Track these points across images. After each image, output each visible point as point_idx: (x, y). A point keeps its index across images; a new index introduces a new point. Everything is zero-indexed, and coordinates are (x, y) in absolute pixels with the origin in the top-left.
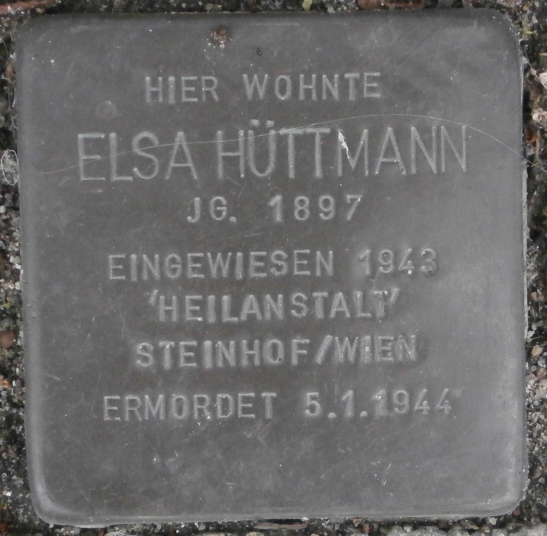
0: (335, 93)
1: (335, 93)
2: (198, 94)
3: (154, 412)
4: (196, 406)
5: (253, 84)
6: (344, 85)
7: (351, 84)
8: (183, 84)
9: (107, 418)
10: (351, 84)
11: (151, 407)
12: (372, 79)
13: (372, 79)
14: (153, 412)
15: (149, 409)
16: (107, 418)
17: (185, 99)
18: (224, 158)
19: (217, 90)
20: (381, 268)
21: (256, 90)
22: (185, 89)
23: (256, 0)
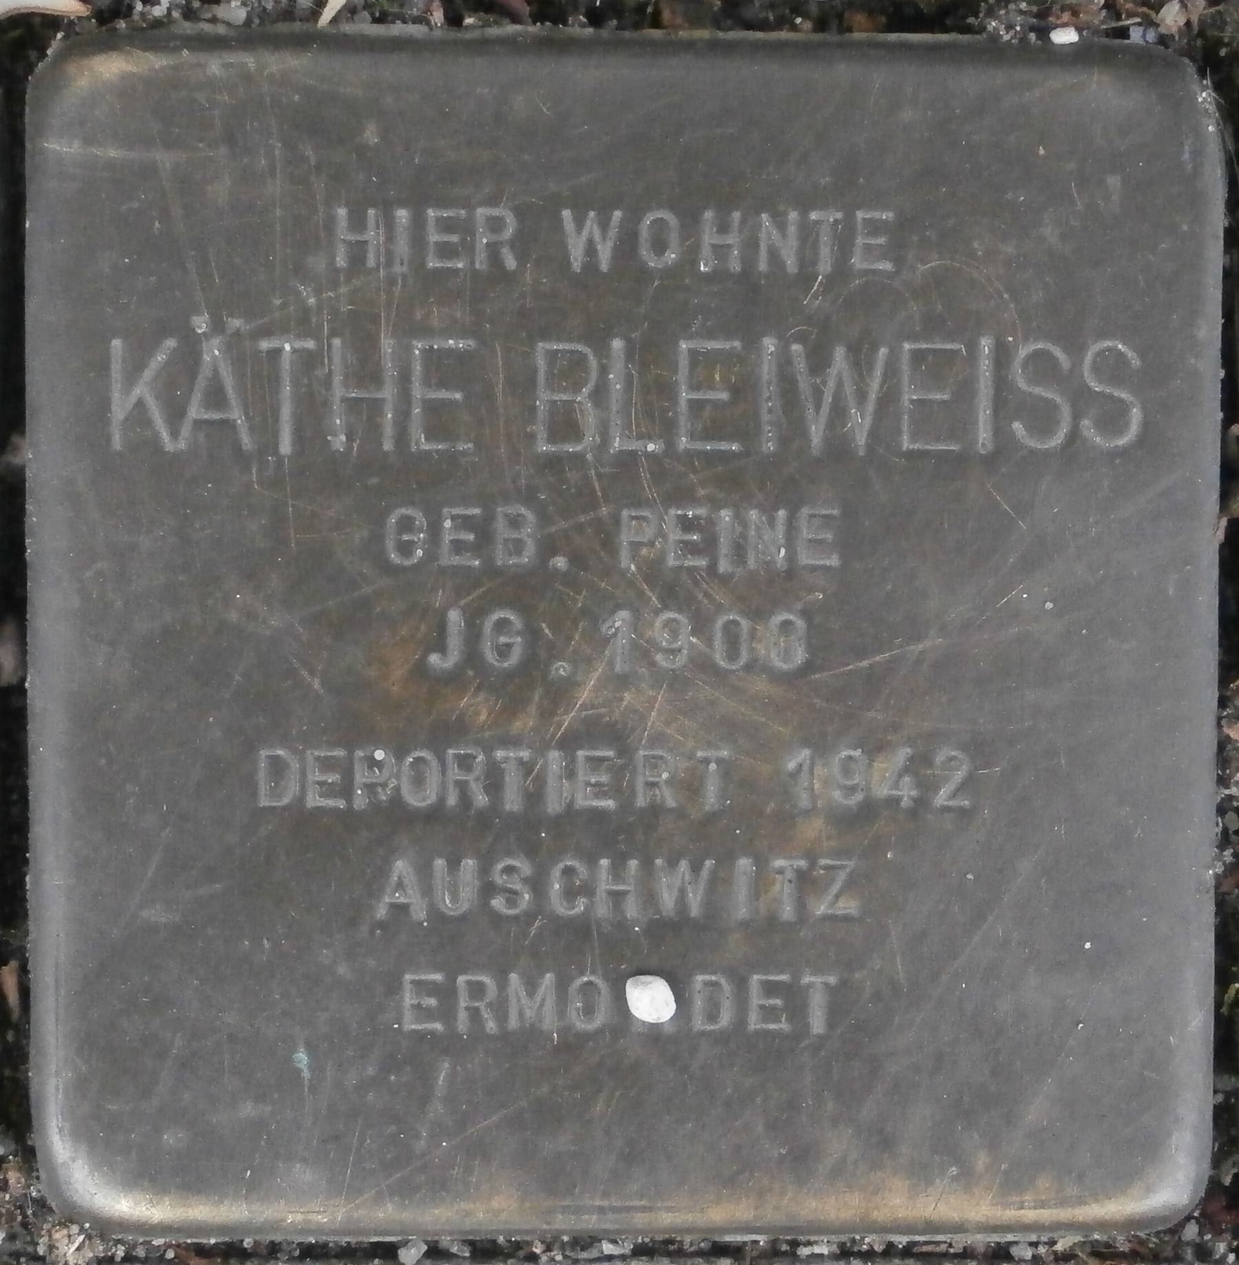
5: (585, 233)
12: (874, 227)
13: (874, 227)
21: (591, 250)
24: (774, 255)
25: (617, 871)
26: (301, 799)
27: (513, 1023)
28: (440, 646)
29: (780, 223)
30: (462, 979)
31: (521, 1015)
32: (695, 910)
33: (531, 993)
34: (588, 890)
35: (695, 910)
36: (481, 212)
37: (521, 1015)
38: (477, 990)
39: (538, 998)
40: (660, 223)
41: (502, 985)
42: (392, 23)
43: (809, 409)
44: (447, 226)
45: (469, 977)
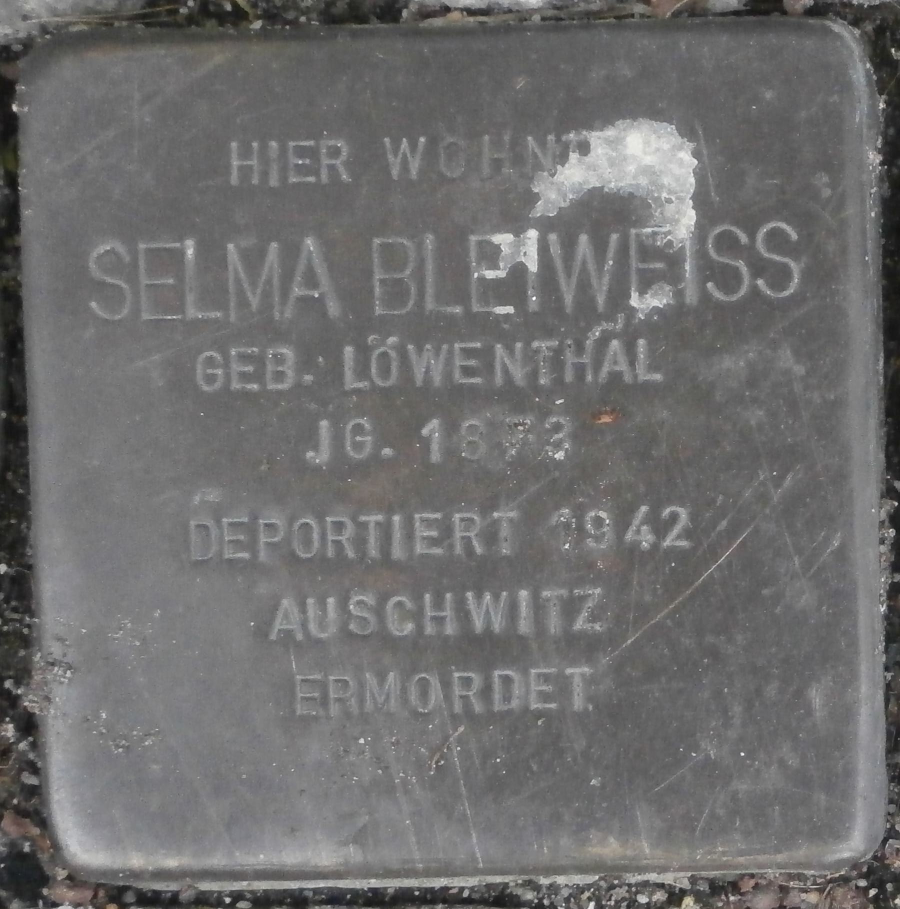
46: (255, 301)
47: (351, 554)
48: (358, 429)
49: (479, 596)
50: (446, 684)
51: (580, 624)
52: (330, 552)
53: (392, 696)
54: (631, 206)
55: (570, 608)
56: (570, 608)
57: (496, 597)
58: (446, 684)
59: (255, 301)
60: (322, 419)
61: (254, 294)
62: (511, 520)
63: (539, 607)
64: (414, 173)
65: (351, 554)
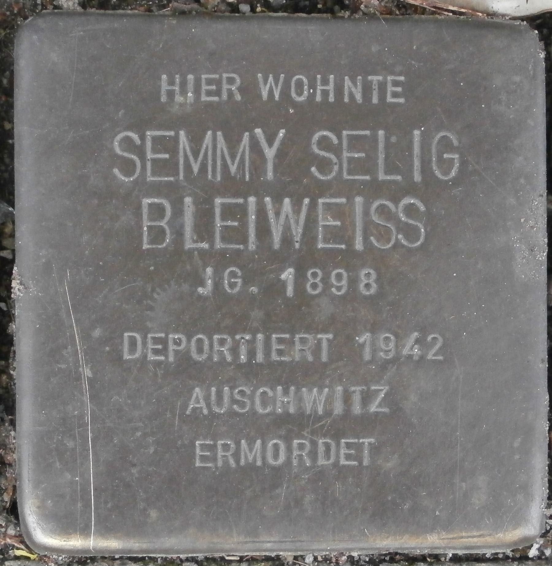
0: (359, 97)
1: (359, 97)
2: (218, 93)
3: (251, 458)
4: (296, 453)
5: (268, 86)
6: (367, 89)
7: (375, 87)
8: (203, 82)
9: (198, 464)
10: (375, 87)
11: (247, 452)
12: (396, 84)
13: (396, 84)
14: (320, 461)
15: (245, 453)
16: (198, 464)
17: (204, 98)
18: (154, 161)
19: (240, 89)
20: (333, 290)
21: (271, 92)
22: (204, 87)
23: (48, 0)
24: (351, 96)
25: (286, 392)
26: (145, 356)
27: (242, 462)
28: (202, 284)
29: (354, 81)
30: (220, 442)
31: (246, 457)
32: (320, 411)
33: (251, 450)
34: (274, 401)
35: (320, 411)
36: (225, 75)
37: (246, 457)
38: (226, 447)
39: (253, 453)
40: (300, 94)
41: (238, 444)
42: (430, 554)
43: (228, 359)
44: (209, 82)
45: (328, 200)
46: (196, 168)
47: (229, 358)
48: (233, 275)
49: (310, 390)
50: (289, 449)
51: (373, 408)
52: (318, 98)
53: (258, 450)
54: (372, 12)
55: (367, 398)
56: (367, 398)
57: (320, 392)
58: (289, 449)
59: (196, 168)
60: (251, 195)
61: (196, 162)
62: (328, 340)
63: (347, 398)
64: (277, 97)
65: (229, 358)
